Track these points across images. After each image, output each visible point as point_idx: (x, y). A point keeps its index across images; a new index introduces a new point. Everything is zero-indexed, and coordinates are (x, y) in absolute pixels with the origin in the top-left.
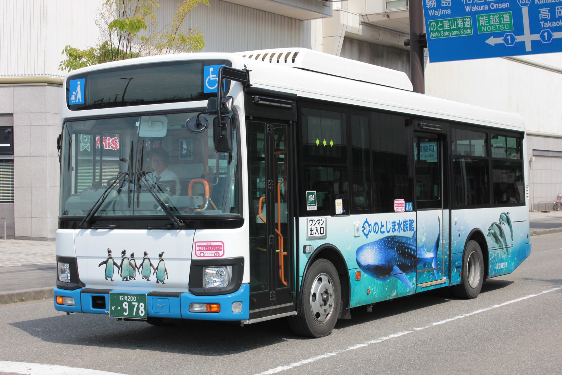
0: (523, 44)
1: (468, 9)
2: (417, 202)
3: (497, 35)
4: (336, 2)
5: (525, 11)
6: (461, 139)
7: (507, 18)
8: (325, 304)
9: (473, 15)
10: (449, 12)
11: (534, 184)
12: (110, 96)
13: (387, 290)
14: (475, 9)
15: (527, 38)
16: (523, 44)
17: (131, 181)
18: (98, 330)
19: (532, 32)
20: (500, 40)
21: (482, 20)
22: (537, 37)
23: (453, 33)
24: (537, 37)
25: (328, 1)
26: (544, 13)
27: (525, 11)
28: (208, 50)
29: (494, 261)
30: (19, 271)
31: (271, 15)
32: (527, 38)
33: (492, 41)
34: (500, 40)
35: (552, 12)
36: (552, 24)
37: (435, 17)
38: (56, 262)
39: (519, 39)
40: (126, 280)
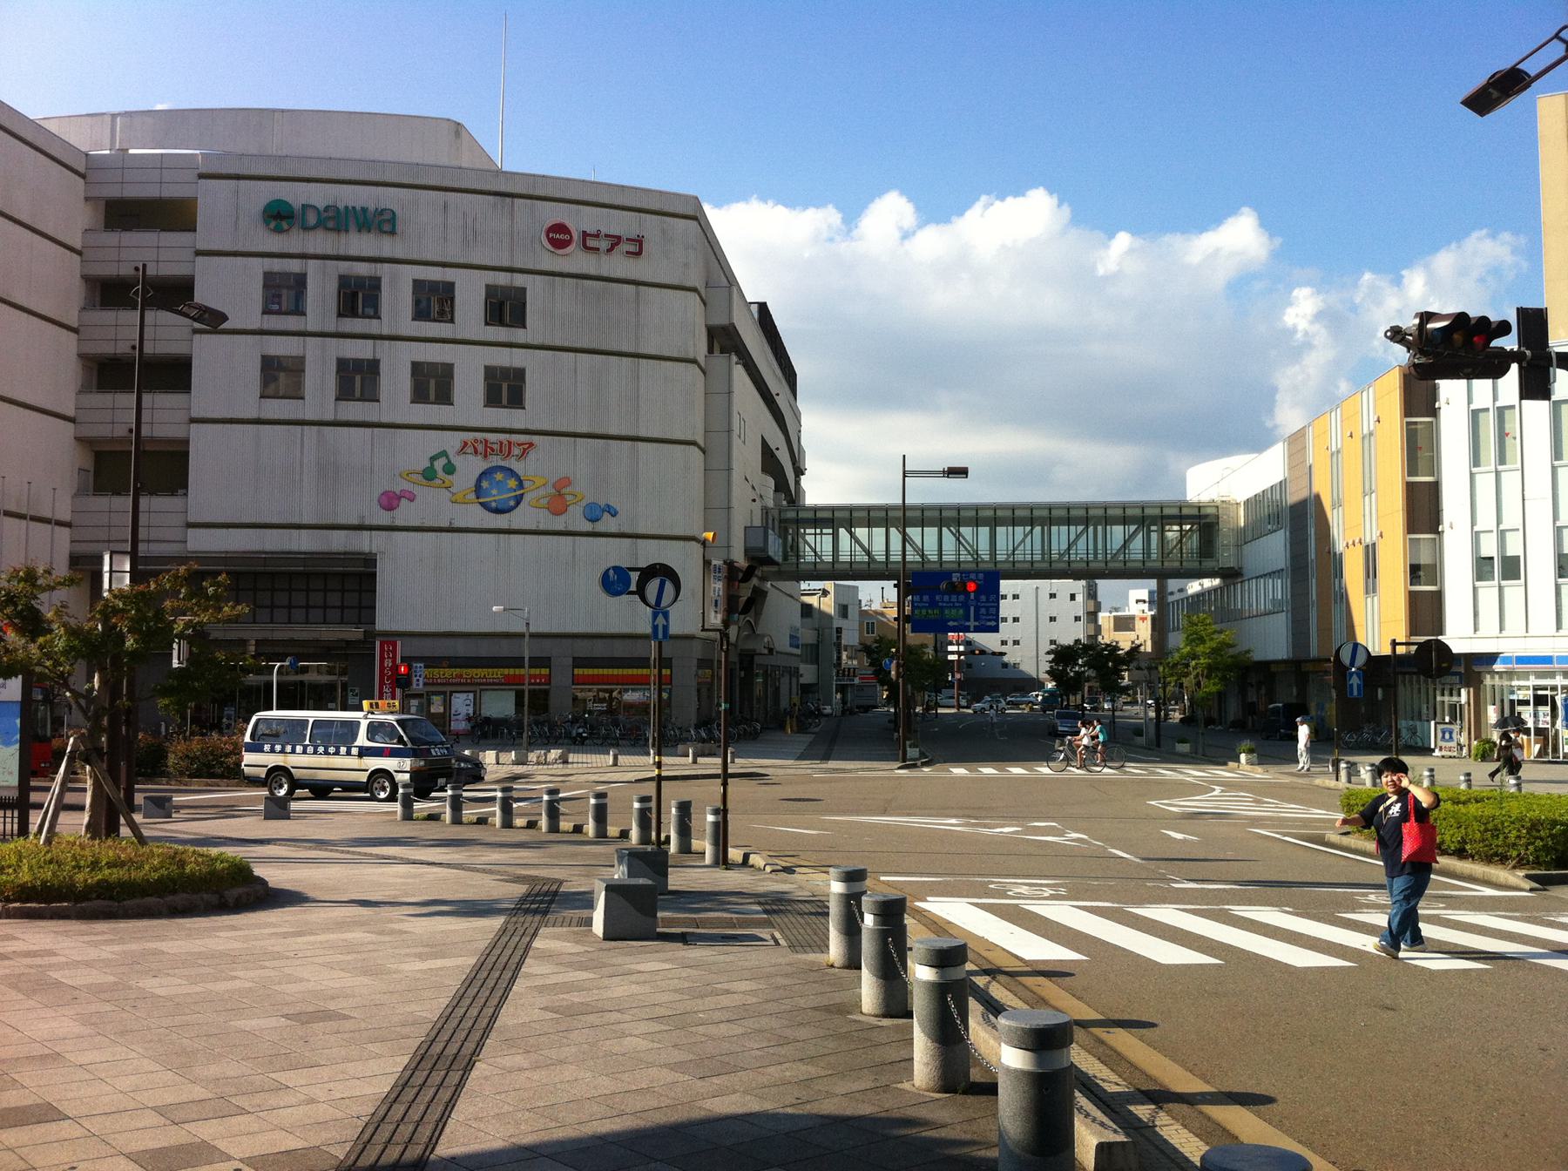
0: (969, 626)
1: (940, 604)
2: (530, 667)
3: (954, 621)
5: (972, 609)
6: (100, 677)
7: (961, 611)
12: (1333, 857)
15: (972, 623)
16: (969, 626)
17: (287, 297)
19: (523, 691)
20: (955, 624)
21: (947, 612)
22: (977, 624)
24: (977, 624)
26: (983, 611)
27: (972, 609)
29: (130, 610)
30: (418, 1094)
32: (972, 623)
33: (951, 624)
35: (987, 611)
36: (1201, 585)
37: (918, 607)
38: (640, 566)
39: (967, 624)
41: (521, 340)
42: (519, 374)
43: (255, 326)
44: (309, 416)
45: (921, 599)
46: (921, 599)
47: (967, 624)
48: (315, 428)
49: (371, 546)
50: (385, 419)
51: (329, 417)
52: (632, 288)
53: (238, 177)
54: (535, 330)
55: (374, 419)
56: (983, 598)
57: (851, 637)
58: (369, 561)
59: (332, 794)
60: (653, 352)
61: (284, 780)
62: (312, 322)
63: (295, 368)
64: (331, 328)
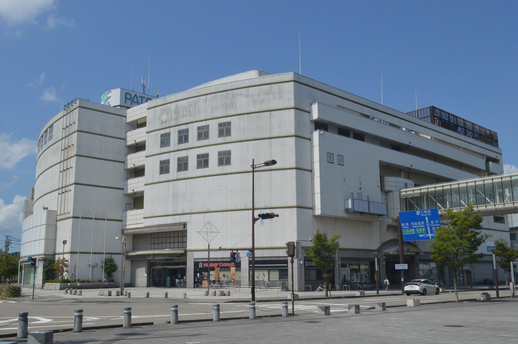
1: (413, 227)
3: (422, 234)
5: (428, 228)
7: (424, 229)
10: (408, 227)
14: (415, 227)
22: (432, 235)
23: (410, 233)
26: (434, 228)
27: (428, 228)
39: (428, 235)
41: (229, 141)
42: (229, 153)
43: (158, 152)
44: (171, 178)
45: (405, 224)
46: (405, 224)
47: (428, 235)
48: (172, 182)
49: (186, 220)
50: (190, 176)
51: (175, 178)
52: (268, 113)
53: (155, 107)
54: (235, 135)
55: (186, 176)
56: (432, 222)
57: (312, 254)
58: (185, 225)
59: (426, 294)
60: (266, 140)
61: (441, 280)
62: (216, 123)
63: (221, 134)
64: (176, 149)
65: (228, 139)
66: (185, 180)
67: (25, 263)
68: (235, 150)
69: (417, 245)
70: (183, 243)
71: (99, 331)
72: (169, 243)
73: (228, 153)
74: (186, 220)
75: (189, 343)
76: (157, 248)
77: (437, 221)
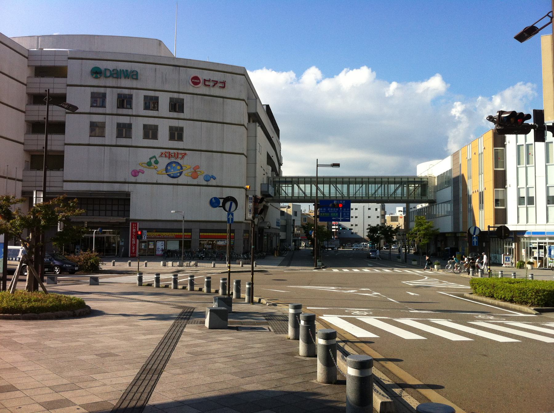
4: (150, 185)
7: (337, 214)
8: (421, 241)
9: (330, 213)
11: (51, 186)
13: (485, 246)
15: (341, 218)
18: (283, 236)
20: (335, 218)
22: (342, 218)
24: (342, 218)
25: (110, 408)
26: (345, 214)
28: (527, 244)
31: (499, 242)
33: (333, 218)
34: (335, 218)
35: (346, 214)
39: (339, 218)
40: (234, 233)
45: (323, 209)
46: (323, 209)
47: (339, 218)
49: (128, 189)
54: (186, 114)
55: (130, 144)
56: (345, 209)
62: (108, 110)
65: (181, 115)
66: (128, 148)
67: (227, 283)
68: (189, 129)
69: (438, 229)
70: (117, 212)
71: (20, 323)
72: (92, 210)
73: (181, 129)
74: (128, 189)
75: (2, 285)
76: (92, 215)
77: (324, 209)
